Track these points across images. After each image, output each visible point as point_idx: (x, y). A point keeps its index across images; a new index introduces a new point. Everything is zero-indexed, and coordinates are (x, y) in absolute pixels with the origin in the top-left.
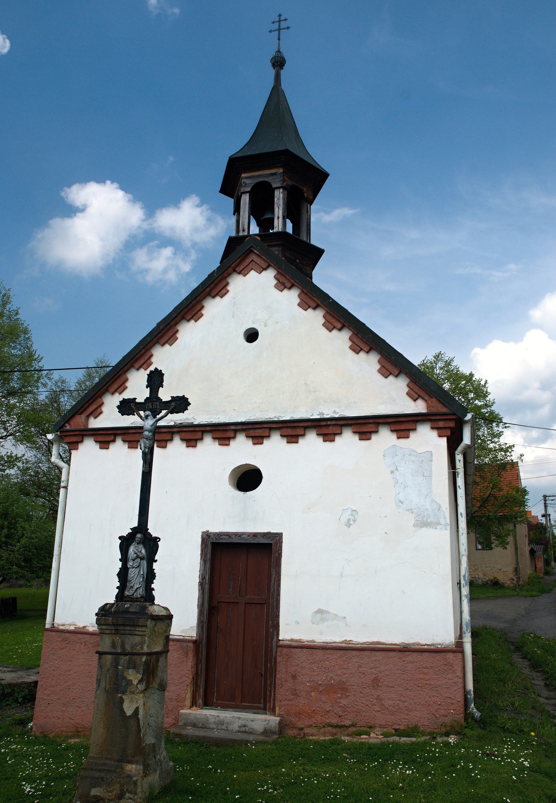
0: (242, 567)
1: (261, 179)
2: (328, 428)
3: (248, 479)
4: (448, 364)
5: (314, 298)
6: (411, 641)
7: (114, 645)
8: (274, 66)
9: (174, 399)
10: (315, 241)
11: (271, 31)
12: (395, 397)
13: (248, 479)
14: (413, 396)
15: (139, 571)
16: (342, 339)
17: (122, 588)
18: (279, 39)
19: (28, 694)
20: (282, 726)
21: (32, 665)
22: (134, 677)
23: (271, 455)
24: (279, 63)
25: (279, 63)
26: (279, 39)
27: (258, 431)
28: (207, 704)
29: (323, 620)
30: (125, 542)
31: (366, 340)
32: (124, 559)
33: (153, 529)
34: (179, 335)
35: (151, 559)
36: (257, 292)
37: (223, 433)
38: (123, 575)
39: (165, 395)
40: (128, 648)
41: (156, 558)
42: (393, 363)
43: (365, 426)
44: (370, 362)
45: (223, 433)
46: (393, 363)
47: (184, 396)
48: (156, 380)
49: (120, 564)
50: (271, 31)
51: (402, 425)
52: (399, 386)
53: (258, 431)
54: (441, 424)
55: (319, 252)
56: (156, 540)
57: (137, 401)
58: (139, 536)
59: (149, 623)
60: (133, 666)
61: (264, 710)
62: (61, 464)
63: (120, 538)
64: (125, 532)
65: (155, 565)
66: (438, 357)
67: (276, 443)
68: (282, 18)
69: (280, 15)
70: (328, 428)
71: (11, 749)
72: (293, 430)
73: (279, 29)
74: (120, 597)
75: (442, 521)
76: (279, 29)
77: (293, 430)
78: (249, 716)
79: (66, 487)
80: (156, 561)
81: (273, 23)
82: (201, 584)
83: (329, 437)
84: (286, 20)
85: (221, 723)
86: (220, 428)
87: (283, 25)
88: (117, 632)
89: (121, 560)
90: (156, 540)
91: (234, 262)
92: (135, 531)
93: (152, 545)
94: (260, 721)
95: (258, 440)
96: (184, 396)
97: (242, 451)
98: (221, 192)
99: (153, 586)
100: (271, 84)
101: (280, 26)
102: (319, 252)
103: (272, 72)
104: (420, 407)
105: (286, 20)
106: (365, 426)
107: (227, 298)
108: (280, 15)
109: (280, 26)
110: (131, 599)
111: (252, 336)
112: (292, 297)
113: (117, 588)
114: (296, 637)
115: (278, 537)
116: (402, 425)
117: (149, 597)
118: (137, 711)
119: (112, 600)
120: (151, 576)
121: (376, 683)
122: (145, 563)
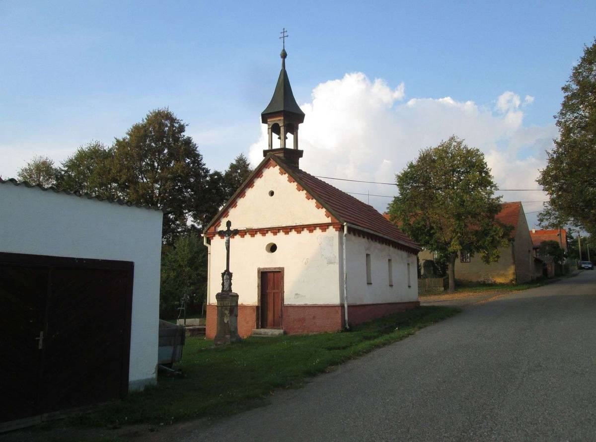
0: (270, 280)
1: (275, 122)
2: (299, 229)
3: (273, 248)
4: (459, 143)
6: (326, 303)
7: (221, 304)
8: (282, 57)
10: (300, 148)
17: (223, 288)
20: (285, 333)
22: (227, 312)
23: (280, 239)
24: (284, 55)
25: (284, 55)
27: (275, 230)
28: (263, 327)
29: (298, 297)
30: (223, 275)
32: (223, 280)
33: (231, 271)
34: (246, 194)
35: (230, 279)
37: (264, 231)
38: (223, 284)
39: (232, 228)
40: (225, 305)
43: (311, 228)
45: (264, 231)
48: (229, 224)
49: (222, 281)
50: (280, 38)
51: (324, 227)
53: (275, 230)
54: (336, 226)
59: (230, 298)
60: (226, 309)
61: (279, 329)
62: (207, 245)
64: (223, 271)
65: (232, 281)
66: (452, 139)
67: (281, 234)
68: (285, 30)
69: (284, 29)
70: (299, 229)
71: (158, 166)
72: (287, 230)
73: (284, 37)
74: (223, 290)
75: (336, 262)
76: (284, 37)
77: (287, 230)
78: (273, 330)
79: (210, 254)
81: (281, 33)
82: (258, 286)
85: (265, 333)
88: (222, 301)
92: (226, 271)
93: (230, 275)
94: (277, 332)
95: (275, 234)
97: (270, 238)
103: (281, 60)
106: (311, 228)
107: (263, 178)
108: (284, 29)
110: (225, 291)
111: (272, 194)
114: (289, 303)
115: (259, 270)
116: (324, 227)
117: (230, 290)
118: (228, 321)
119: (220, 292)
120: (230, 284)
121: (314, 317)
122: (229, 281)
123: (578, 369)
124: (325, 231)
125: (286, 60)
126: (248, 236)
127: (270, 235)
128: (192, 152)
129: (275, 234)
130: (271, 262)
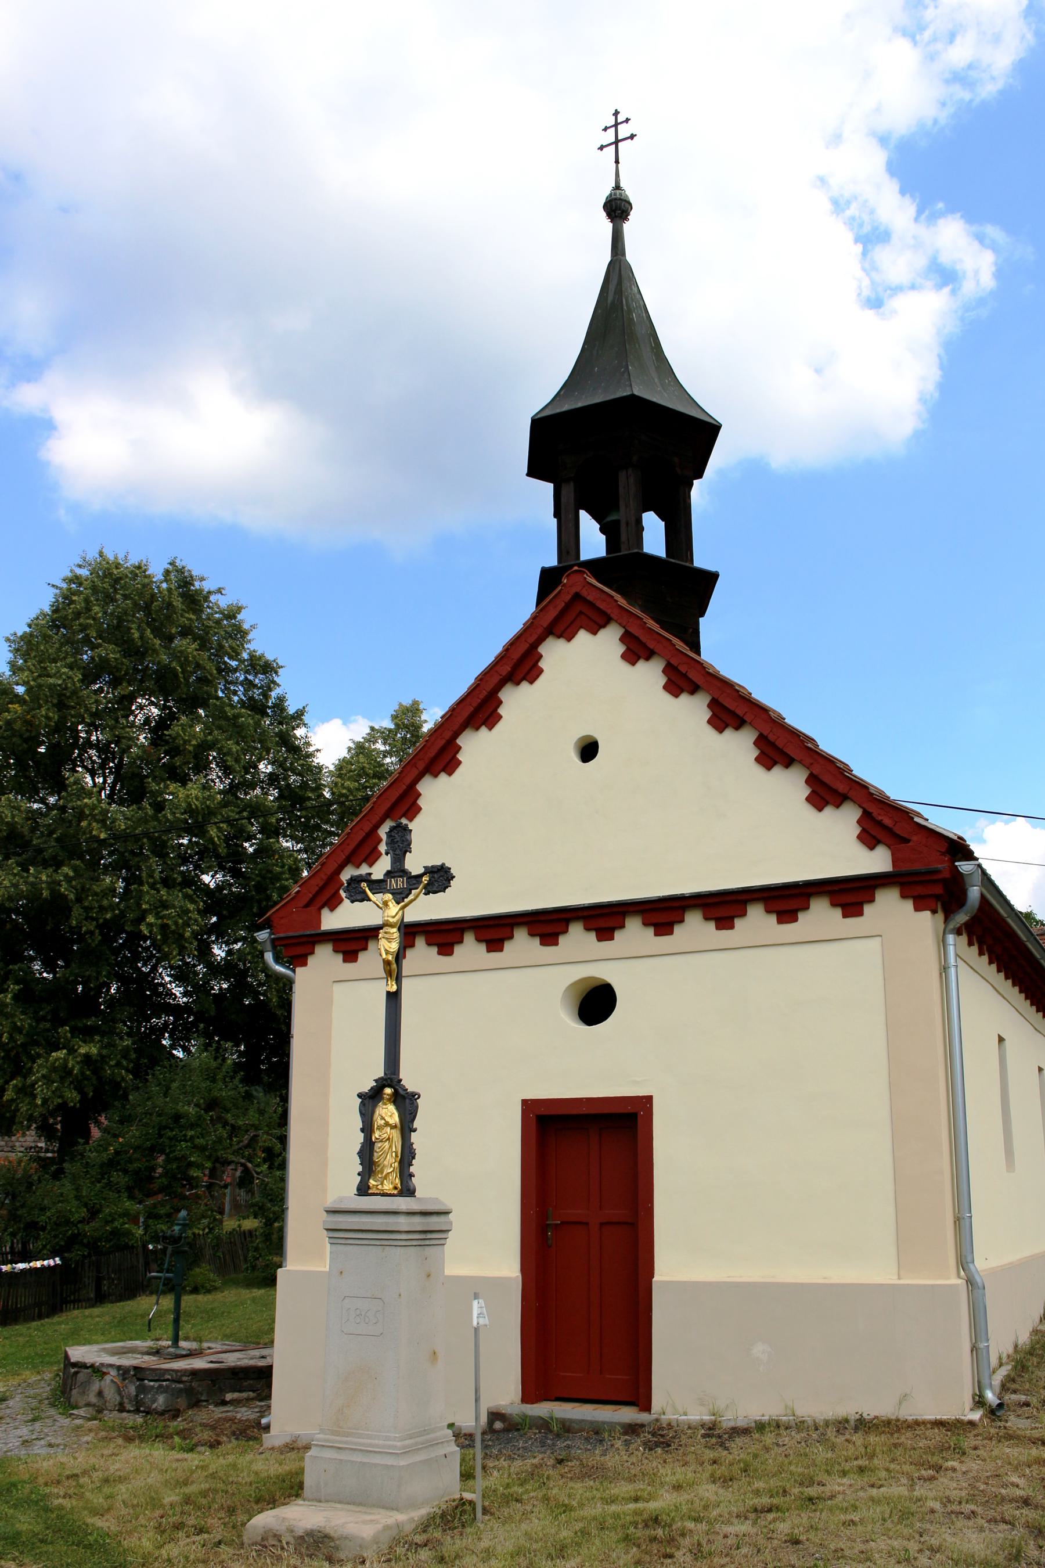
3: (596, 1004)
5: (686, 677)
9: (430, 871)
10: (702, 560)
11: (601, 148)
12: (835, 847)
13: (596, 1004)
14: (869, 838)
15: (391, 1147)
16: (739, 746)
18: (617, 162)
19: (258, 1381)
21: (264, 1337)
23: (627, 961)
24: (617, 209)
25: (617, 209)
26: (617, 162)
30: (370, 1099)
31: (780, 745)
32: (368, 1128)
33: (409, 1080)
35: (406, 1127)
36: (589, 668)
41: (416, 1125)
42: (832, 785)
43: (786, 901)
44: (789, 785)
45: (548, 925)
46: (832, 785)
47: (443, 864)
49: (360, 1137)
50: (601, 148)
51: (850, 894)
52: (842, 824)
53: (604, 919)
55: (710, 579)
56: (414, 1097)
57: (373, 877)
58: (388, 1091)
63: (360, 1096)
64: (367, 1085)
67: (634, 934)
68: (620, 119)
70: (723, 907)
76: (617, 142)
77: (663, 914)
80: (415, 1130)
81: (605, 129)
83: (725, 922)
84: (627, 120)
86: (542, 918)
87: (624, 131)
89: (362, 1130)
90: (414, 1097)
91: (604, 592)
93: (408, 1104)
95: (605, 934)
96: (443, 864)
97: (581, 957)
98: (528, 475)
99: (412, 1169)
100: (607, 258)
101: (617, 135)
102: (710, 579)
103: (607, 227)
104: (877, 861)
105: (627, 120)
109: (617, 135)
111: (588, 751)
112: (650, 675)
113: (359, 1174)
115: (525, 1102)
116: (850, 894)
123: (843, 1485)
124: (860, 913)
125: (627, 227)
126: (470, 950)
127: (577, 939)
128: (161, 989)
129: (605, 934)
130: (588, 1068)
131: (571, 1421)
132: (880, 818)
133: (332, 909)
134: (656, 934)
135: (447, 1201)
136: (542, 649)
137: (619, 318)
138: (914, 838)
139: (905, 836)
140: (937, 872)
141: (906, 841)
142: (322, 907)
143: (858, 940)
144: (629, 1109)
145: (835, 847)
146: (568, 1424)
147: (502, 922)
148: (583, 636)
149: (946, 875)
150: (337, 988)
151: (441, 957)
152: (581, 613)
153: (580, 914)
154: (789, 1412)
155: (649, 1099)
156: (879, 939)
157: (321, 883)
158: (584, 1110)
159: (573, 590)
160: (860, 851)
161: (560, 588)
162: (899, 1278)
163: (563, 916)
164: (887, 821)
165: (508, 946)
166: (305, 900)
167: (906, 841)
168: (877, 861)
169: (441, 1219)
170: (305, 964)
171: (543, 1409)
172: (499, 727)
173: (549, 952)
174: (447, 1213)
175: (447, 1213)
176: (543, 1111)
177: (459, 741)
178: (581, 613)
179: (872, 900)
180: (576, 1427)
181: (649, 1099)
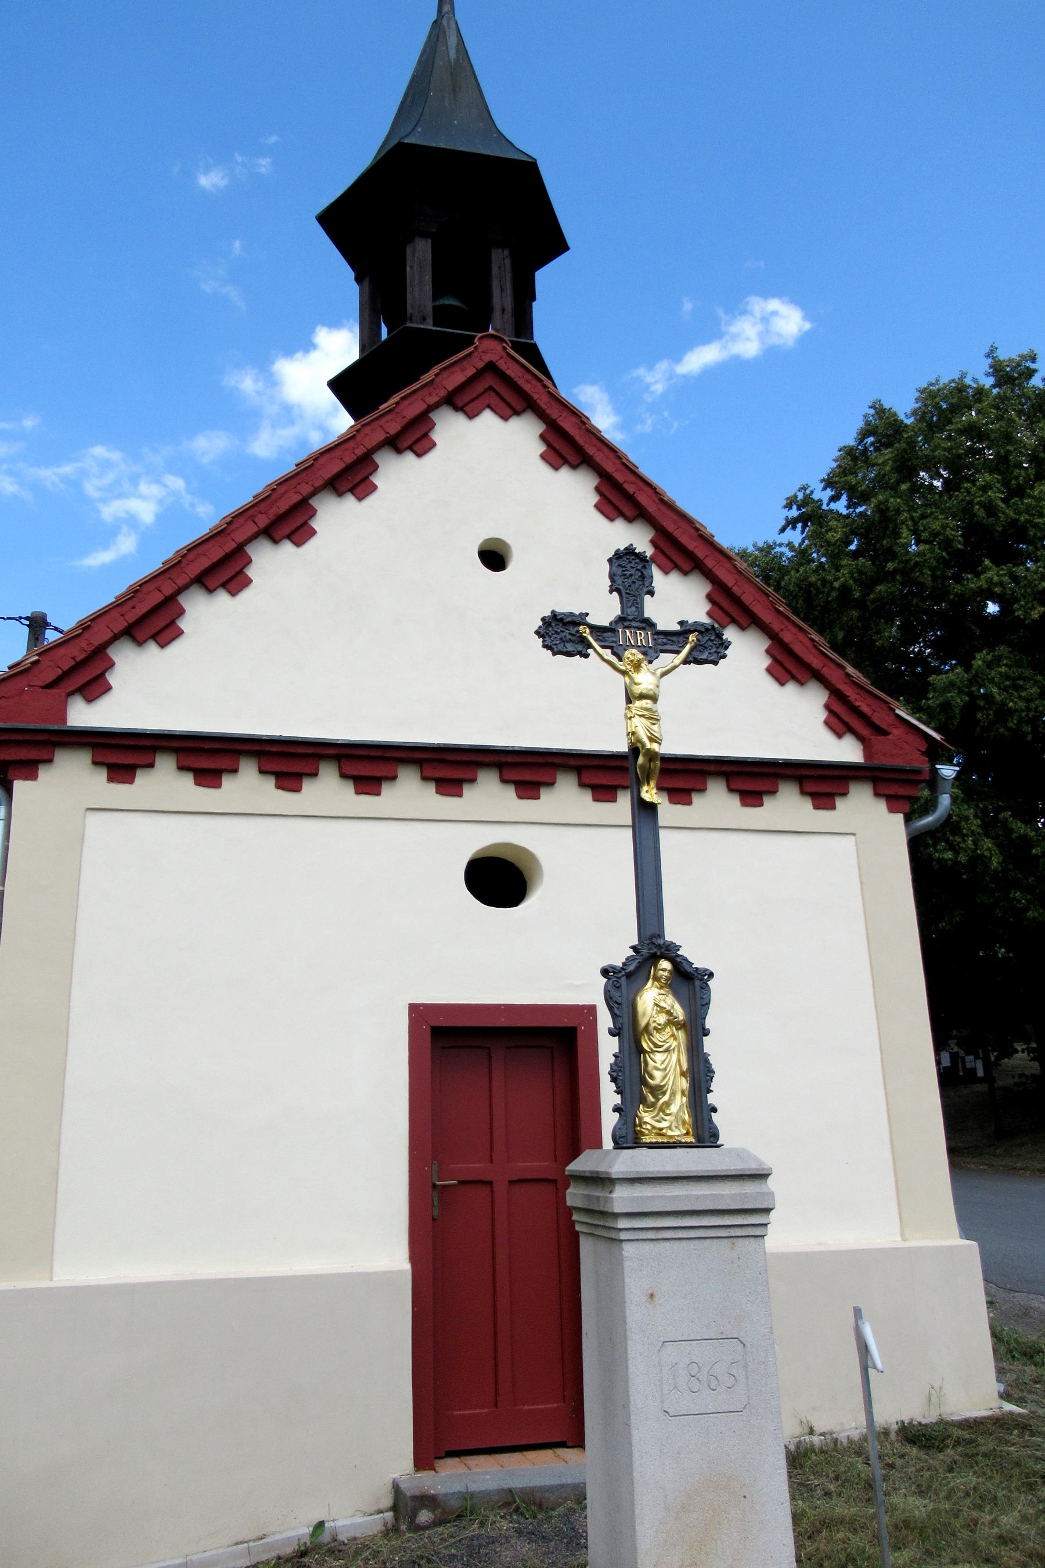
12: (143, 692)
16: (270, 563)
45: (451, 767)
51: (821, 783)
70: (289, 761)
97: (492, 816)
104: (848, 751)
116: (821, 783)
131: (544, 1489)
132: (857, 704)
133: (90, 700)
134: (111, 779)
135: (764, 1156)
136: (435, 416)
137: (442, 71)
138: (896, 732)
139: (884, 727)
140: (918, 772)
141: (885, 733)
142: (71, 694)
143: (442, 824)
144: (565, 1022)
145: (143, 692)
146: (538, 1495)
147: (389, 754)
148: (488, 418)
149: (927, 776)
150: (93, 818)
151: (281, 792)
152: (491, 388)
153: (724, 768)
154: (807, 1430)
155: (414, 1008)
156: (853, 838)
157: (81, 657)
158: (503, 1022)
159: (487, 358)
160: (827, 736)
161: (471, 349)
162: (904, 1239)
163: (844, 773)
164: (865, 709)
165: (307, 785)
166: (50, 676)
167: (885, 733)
168: (848, 751)
169: (750, 1188)
170: (34, 777)
171: (453, 1478)
172: (371, 500)
173: (448, 805)
174: (761, 1176)
175: (761, 1176)
176: (442, 1022)
177: (314, 502)
178: (491, 388)
179: (844, 794)
180: (552, 1498)
181: (414, 1008)
